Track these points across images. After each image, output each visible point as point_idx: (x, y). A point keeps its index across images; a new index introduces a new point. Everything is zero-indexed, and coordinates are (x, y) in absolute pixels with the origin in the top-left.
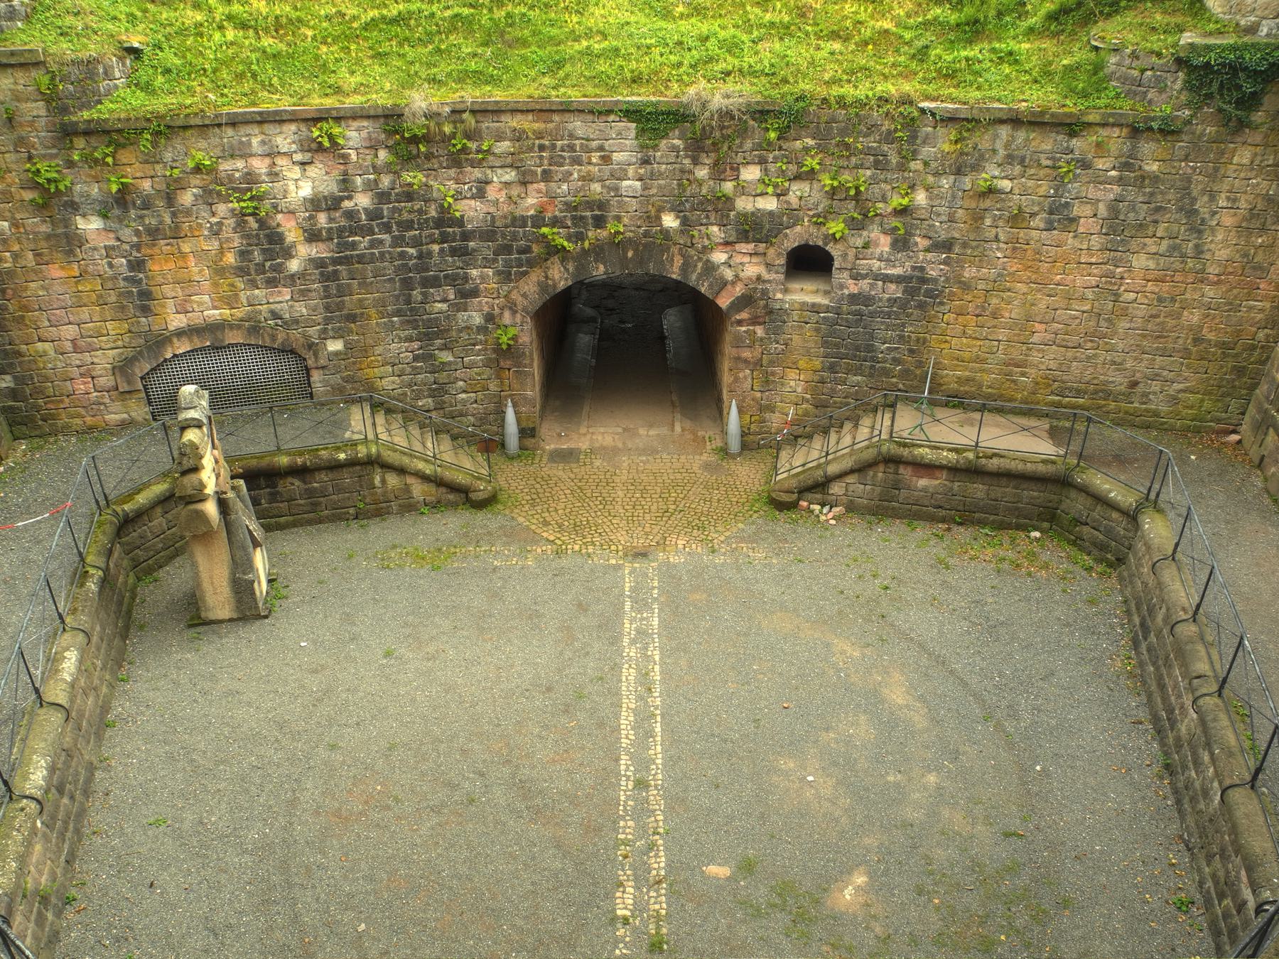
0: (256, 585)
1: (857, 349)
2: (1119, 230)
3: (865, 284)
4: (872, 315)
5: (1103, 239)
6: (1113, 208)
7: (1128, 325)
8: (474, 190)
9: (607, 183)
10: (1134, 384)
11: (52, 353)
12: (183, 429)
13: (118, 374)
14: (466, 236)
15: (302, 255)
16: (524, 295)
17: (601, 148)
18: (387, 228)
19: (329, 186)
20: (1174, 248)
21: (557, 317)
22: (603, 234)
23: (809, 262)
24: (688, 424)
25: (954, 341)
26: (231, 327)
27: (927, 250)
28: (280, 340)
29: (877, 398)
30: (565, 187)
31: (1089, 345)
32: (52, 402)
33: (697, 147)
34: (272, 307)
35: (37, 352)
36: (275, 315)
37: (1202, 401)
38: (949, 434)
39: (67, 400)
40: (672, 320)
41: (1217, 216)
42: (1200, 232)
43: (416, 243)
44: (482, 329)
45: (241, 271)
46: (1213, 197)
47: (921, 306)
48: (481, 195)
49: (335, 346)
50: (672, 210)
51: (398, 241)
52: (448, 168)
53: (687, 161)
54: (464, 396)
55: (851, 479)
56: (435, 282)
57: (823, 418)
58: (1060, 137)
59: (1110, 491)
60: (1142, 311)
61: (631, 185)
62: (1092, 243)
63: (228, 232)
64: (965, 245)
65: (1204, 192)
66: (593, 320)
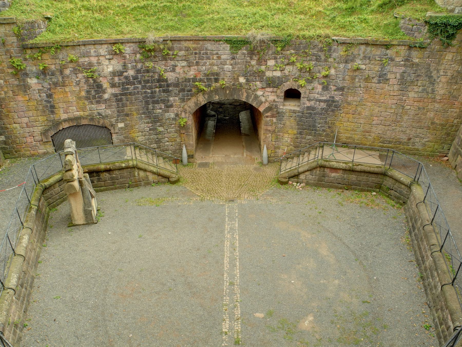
0: (92, 212)
1: (310, 126)
2: (404, 83)
3: (312, 103)
5: (398, 87)
7: (407, 118)
8: (171, 69)
9: (219, 66)
10: (410, 139)
11: (19, 127)
12: (66, 155)
13: (42, 135)
14: (168, 86)
16: (189, 107)
17: (217, 54)
18: (140, 82)
19: (119, 67)
21: (201, 115)
22: (218, 85)
23: (293, 94)
24: (249, 153)
28: (101, 123)
29: (317, 144)
31: (393, 125)
33: (252, 53)
34: (98, 111)
35: (13, 127)
36: (99, 114)
37: (434, 145)
39: (24, 145)
41: (440, 78)
42: (433, 84)
43: (150, 88)
45: (87, 98)
46: (438, 71)
48: (174, 70)
49: (121, 125)
50: (243, 76)
52: (162, 61)
53: (248, 58)
54: (167, 143)
55: (307, 173)
56: (157, 102)
57: (298, 151)
58: (383, 50)
59: (401, 178)
60: (412, 113)
63: (82, 84)
64: (349, 89)
65: (435, 69)
66: (214, 116)
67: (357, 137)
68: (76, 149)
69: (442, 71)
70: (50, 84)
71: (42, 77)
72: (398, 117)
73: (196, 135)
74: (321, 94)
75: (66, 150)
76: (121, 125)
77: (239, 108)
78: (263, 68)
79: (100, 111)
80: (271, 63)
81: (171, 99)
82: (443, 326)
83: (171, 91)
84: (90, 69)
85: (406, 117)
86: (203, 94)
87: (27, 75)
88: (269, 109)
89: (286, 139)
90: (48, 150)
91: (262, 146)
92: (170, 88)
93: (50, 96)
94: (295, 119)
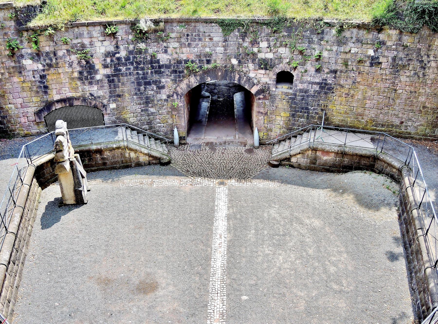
0: (83, 192)
1: (303, 109)
2: (397, 67)
4: (308, 96)
5: (391, 70)
6: (394, 59)
7: (400, 101)
8: (163, 51)
9: (211, 48)
10: (402, 123)
11: (13, 108)
12: (57, 136)
13: (36, 115)
14: (160, 67)
15: (102, 73)
17: (209, 36)
18: (132, 64)
19: (112, 49)
20: (415, 74)
21: (194, 96)
22: (210, 66)
23: (285, 78)
24: (241, 135)
25: (337, 106)
26: (76, 99)
27: (328, 73)
28: (93, 104)
29: (310, 126)
30: (196, 49)
31: (386, 108)
32: (13, 125)
34: (91, 92)
35: (9, 108)
36: (92, 95)
37: (426, 129)
38: (333, 141)
39: (18, 125)
40: (238, 97)
41: (430, 63)
42: (424, 68)
43: (143, 69)
44: (166, 100)
45: (80, 79)
46: (428, 56)
47: (326, 93)
48: (166, 52)
50: (235, 58)
51: (136, 68)
52: (154, 42)
53: (241, 40)
54: (159, 125)
55: (299, 156)
56: (149, 83)
57: (290, 134)
58: (375, 33)
59: (393, 162)
60: (404, 97)
61: (220, 49)
62: (387, 71)
63: (75, 65)
64: (341, 72)
65: (425, 54)
66: (209, 97)
67: (350, 120)
68: (67, 130)
69: (432, 56)
70: (44, 66)
71: (36, 58)
72: (391, 100)
73: (188, 116)
74: (313, 77)
75: (57, 131)
76: (113, 106)
77: (233, 90)
78: (255, 50)
79: (92, 92)
80: (264, 45)
81: (163, 80)
82: (423, 308)
83: (163, 72)
84: (83, 50)
85: (398, 101)
86: (195, 76)
87: (22, 56)
88: (260, 92)
89: (279, 121)
90: (41, 130)
91: (254, 129)
92: (162, 70)
93: (43, 77)
94: (288, 102)
